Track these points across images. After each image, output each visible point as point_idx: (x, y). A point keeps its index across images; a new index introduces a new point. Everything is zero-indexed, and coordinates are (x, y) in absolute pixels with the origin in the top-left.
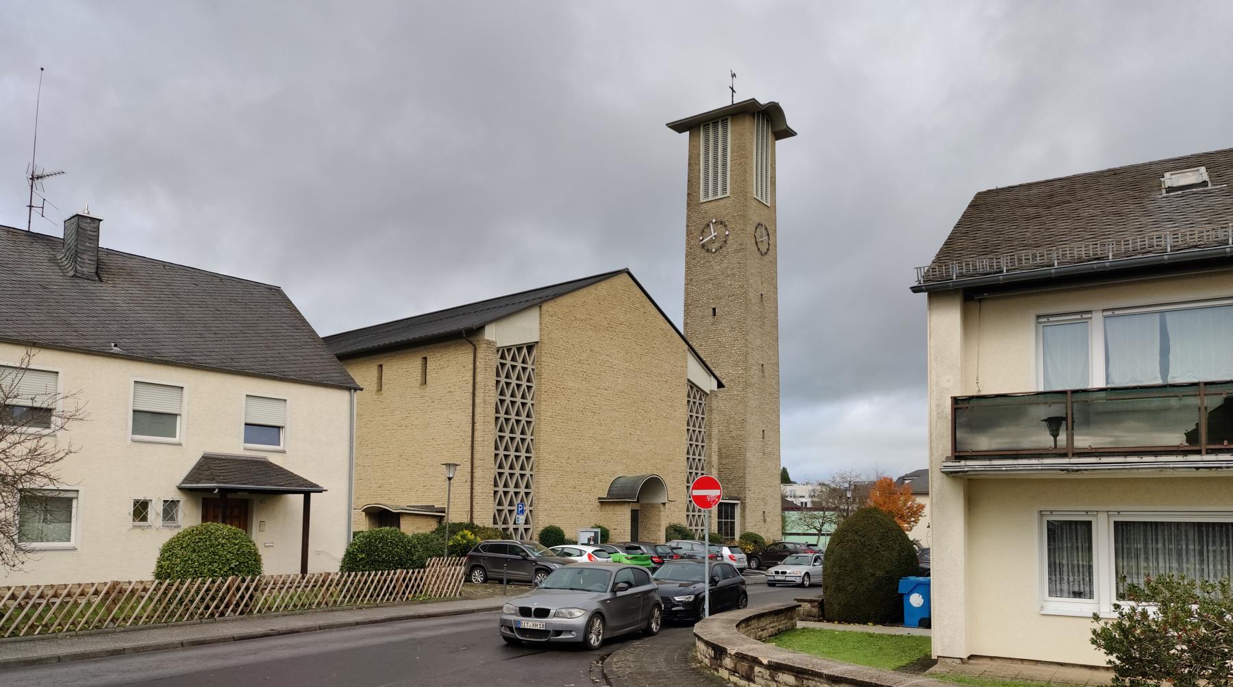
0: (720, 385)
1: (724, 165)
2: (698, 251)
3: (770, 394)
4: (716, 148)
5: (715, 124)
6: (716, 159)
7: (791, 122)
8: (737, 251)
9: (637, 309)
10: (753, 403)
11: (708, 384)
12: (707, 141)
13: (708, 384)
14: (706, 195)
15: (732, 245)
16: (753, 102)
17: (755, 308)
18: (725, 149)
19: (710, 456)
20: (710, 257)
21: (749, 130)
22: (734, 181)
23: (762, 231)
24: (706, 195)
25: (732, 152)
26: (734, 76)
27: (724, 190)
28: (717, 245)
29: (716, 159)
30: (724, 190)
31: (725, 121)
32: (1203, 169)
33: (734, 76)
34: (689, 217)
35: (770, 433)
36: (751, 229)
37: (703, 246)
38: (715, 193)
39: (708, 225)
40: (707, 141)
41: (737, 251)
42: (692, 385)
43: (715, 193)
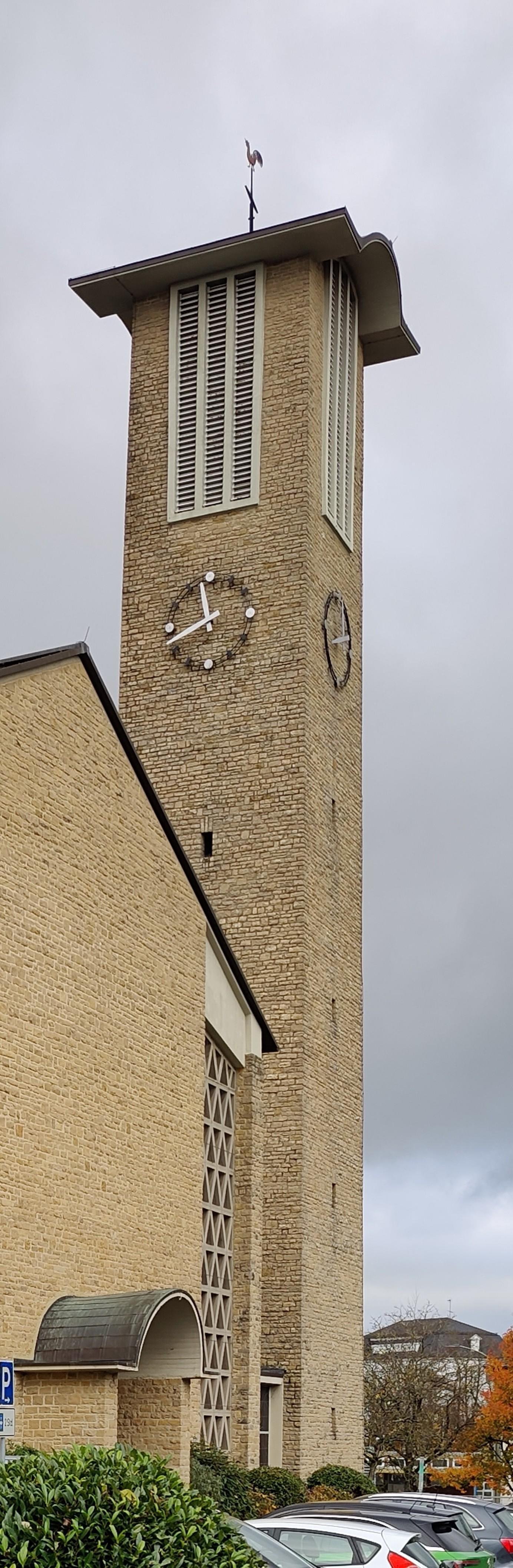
0: (269, 1045)
1: (244, 410)
2: (161, 665)
3: (347, 1085)
4: (343, 354)
5: (188, 293)
6: (216, 395)
7: (416, 311)
8: (278, 668)
9: (102, 780)
10: (314, 1105)
11: (243, 1039)
12: (189, 339)
13: (243, 1039)
14: (187, 499)
15: (265, 650)
16: (338, 222)
17: (322, 838)
18: (245, 364)
19: (245, 1246)
20: (197, 682)
21: (320, 318)
22: (272, 460)
23: (335, 617)
24: (187, 499)
25: (268, 373)
26: (255, 158)
27: (242, 485)
28: (218, 648)
29: (216, 395)
30: (242, 485)
31: (245, 280)
32: (257, 1466)
33: (255, 158)
34: (130, 565)
35: (345, 1196)
36: (316, 605)
37: (175, 651)
38: (214, 493)
39: (192, 591)
40: (189, 339)
41: (278, 668)
42: (212, 1035)
43: (214, 493)
